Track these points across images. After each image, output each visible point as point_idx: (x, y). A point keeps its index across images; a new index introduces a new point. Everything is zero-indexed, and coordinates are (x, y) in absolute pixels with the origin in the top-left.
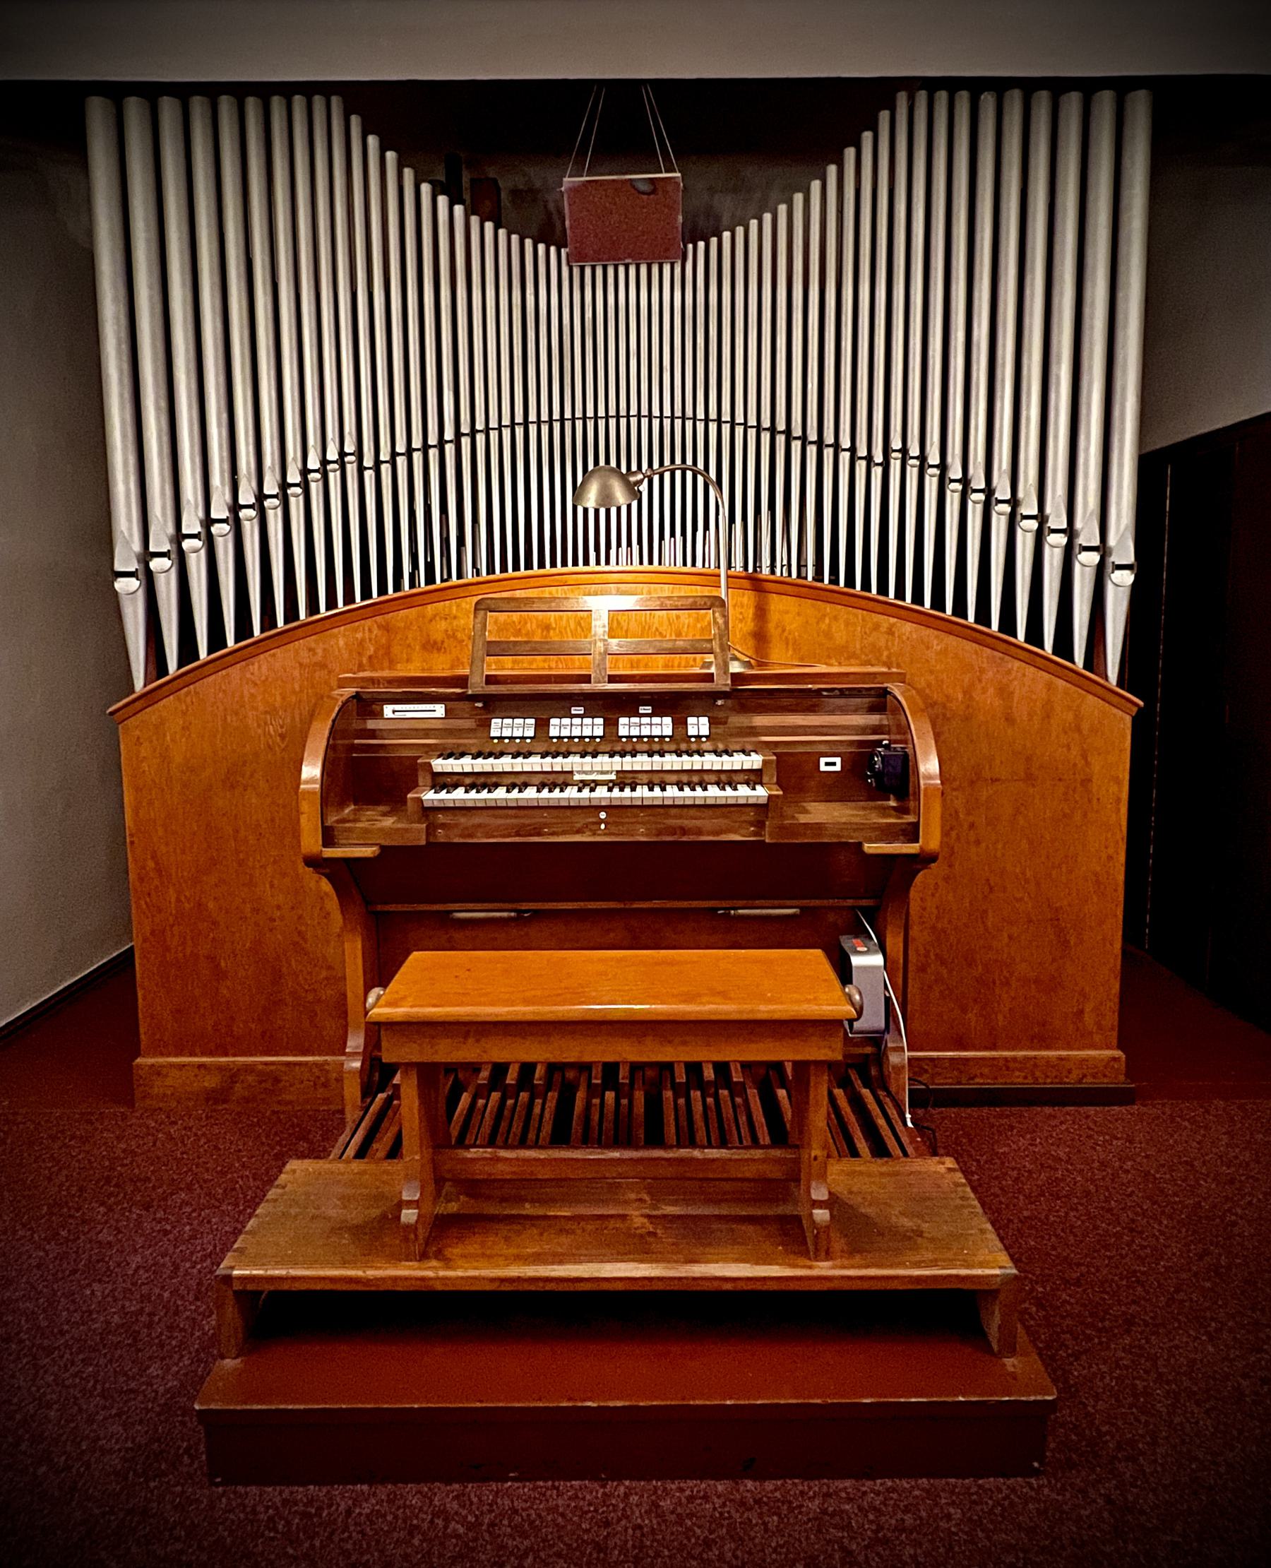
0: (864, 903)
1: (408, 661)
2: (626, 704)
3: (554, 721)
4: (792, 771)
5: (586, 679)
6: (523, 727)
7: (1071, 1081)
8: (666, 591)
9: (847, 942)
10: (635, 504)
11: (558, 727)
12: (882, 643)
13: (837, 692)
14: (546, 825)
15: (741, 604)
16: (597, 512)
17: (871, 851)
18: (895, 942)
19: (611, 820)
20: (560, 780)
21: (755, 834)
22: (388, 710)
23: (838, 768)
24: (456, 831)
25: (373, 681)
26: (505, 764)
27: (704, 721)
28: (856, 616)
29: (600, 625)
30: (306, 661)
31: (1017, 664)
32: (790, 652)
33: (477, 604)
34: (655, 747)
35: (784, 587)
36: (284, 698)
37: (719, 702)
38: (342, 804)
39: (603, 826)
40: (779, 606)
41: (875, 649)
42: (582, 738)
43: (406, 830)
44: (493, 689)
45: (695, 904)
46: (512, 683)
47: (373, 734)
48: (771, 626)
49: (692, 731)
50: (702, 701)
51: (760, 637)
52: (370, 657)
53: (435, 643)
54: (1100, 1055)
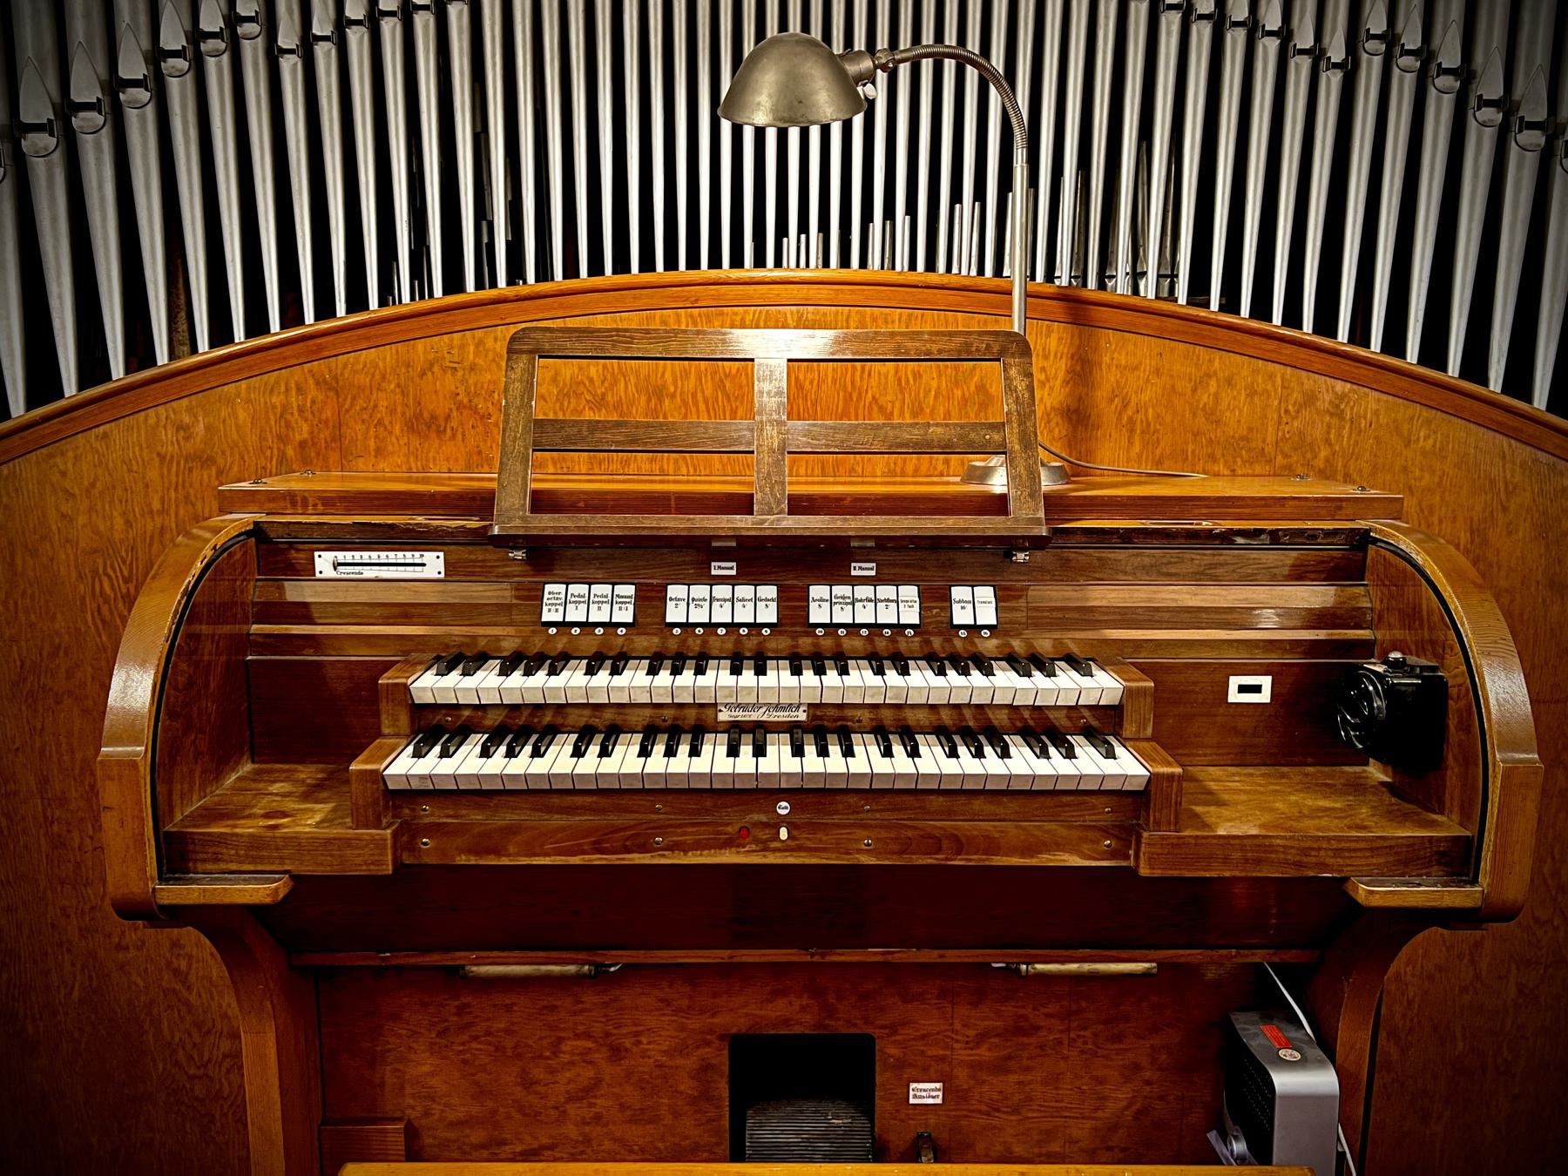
0: (1289, 956)
1: (379, 452)
2: (828, 559)
3: (675, 591)
4: (1173, 704)
5: (743, 504)
6: (604, 603)
8: (897, 321)
9: (1256, 1035)
10: (858, 121)
11: (686, 604)
12: (1318, 433)
15: (1052, 343)
17: (1376, 902)
18: (1352, 1034)
19: (797, 819)
20: (682, 725)
21: (1113, 854)
22: (324, 563)
23: (1265, 697)
25: (292, 499)
26: (572, 682)
27: (986, 593)
28: (1271, 376)
29: (770, 387)
30: (171, 450)
32: (1137, 448)
33: (513, 339)
34: (886, 649)
36: (129, 524)
37: (1021, 557)
38: (221, 763)
39: (784, 833)
41: (1303, 444)
42: (732, 626)
43: (348, 842)
44: (547, 524)
45: (952, 956)
46: (586, 510)
47: (302, 612)
48: (1101, 394)
49: (961, 616)
50: (989, 557)
52: (303, 444)
53: (433, 417)
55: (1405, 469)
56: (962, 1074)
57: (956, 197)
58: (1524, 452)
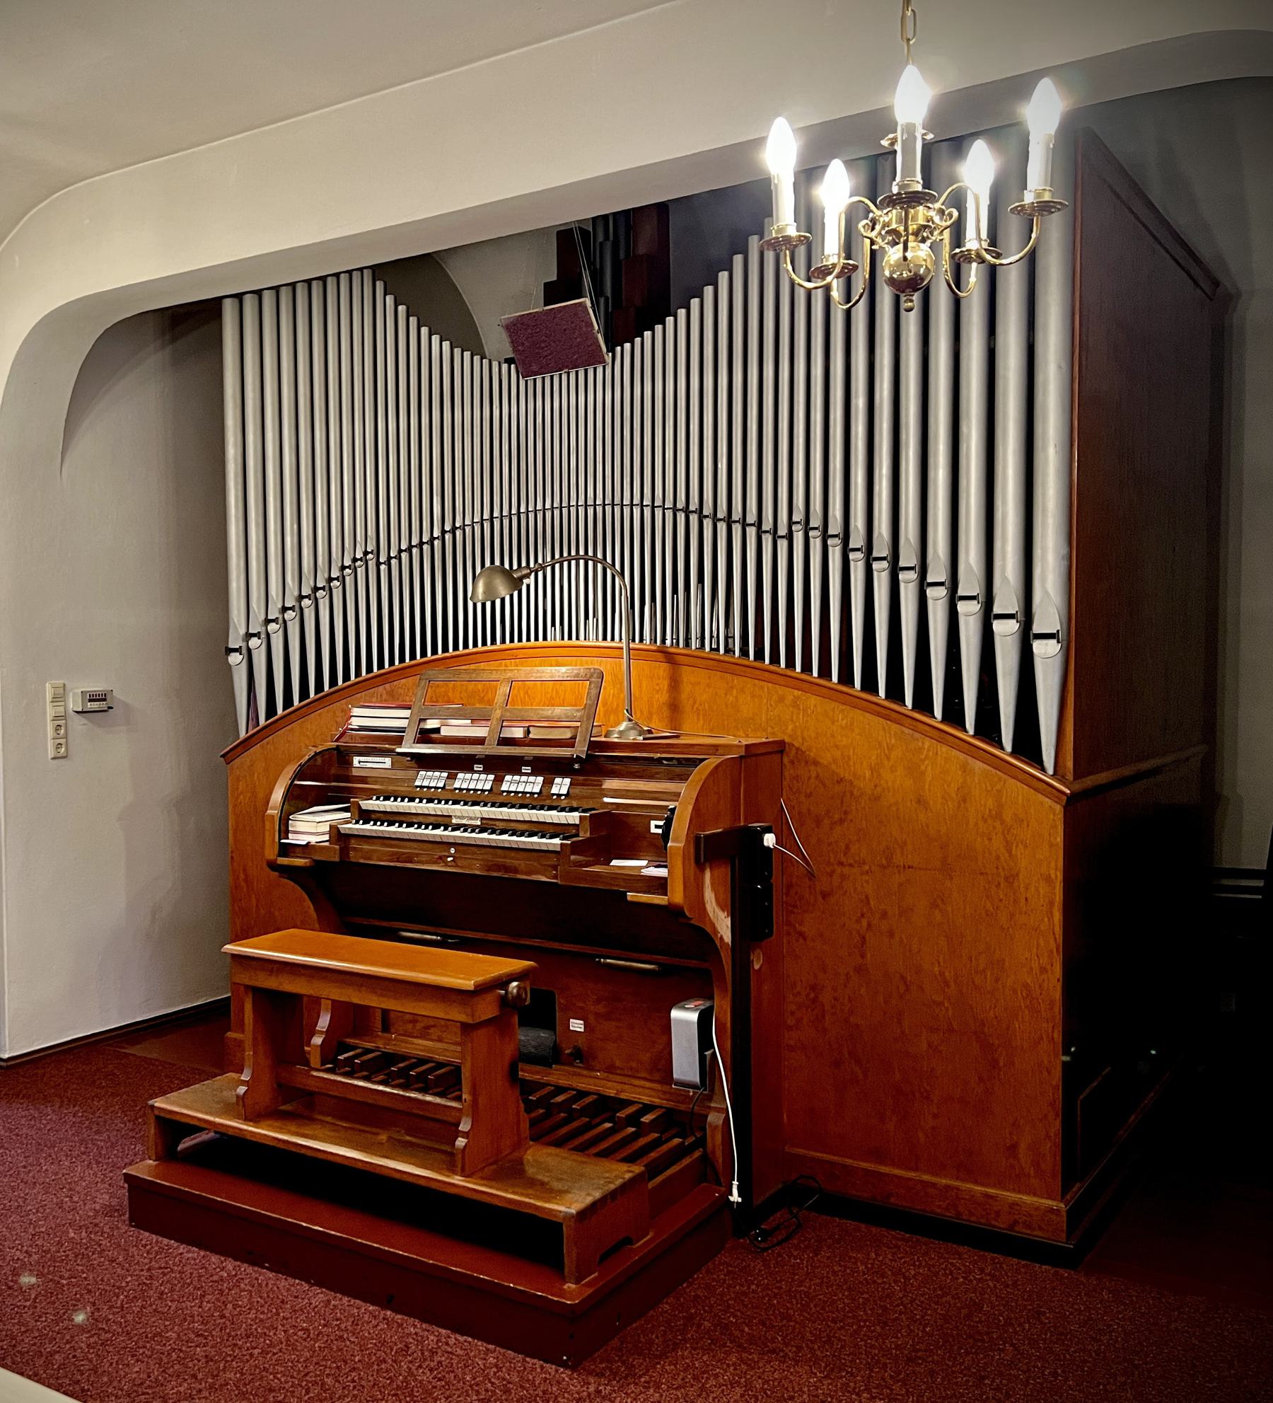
7: (1001, 1224)
10: (516, 594)
13: (675, 762)
14: (417, 855)
16: (484, 606)
20: (442, 822)
22: (356, 760)
24: (360, 854)
31: (928, 742)
34: (524, 801)
35: (700, 661)
40: (689, 676)
45: (556, 946)
48: (684, 696)
49: (555, 790)
51: (674, 708)
54: (1037, 1203)
55: (833, 736)
56: (591, 1018)
57: (587, 617)
58: (894, 727)
